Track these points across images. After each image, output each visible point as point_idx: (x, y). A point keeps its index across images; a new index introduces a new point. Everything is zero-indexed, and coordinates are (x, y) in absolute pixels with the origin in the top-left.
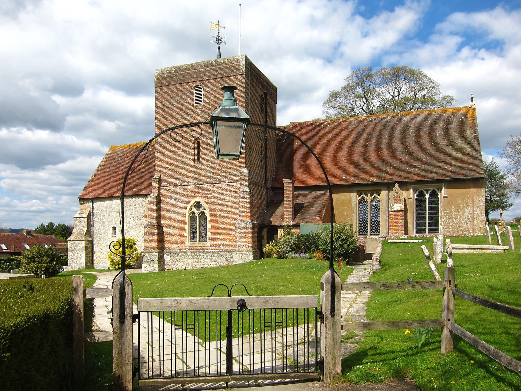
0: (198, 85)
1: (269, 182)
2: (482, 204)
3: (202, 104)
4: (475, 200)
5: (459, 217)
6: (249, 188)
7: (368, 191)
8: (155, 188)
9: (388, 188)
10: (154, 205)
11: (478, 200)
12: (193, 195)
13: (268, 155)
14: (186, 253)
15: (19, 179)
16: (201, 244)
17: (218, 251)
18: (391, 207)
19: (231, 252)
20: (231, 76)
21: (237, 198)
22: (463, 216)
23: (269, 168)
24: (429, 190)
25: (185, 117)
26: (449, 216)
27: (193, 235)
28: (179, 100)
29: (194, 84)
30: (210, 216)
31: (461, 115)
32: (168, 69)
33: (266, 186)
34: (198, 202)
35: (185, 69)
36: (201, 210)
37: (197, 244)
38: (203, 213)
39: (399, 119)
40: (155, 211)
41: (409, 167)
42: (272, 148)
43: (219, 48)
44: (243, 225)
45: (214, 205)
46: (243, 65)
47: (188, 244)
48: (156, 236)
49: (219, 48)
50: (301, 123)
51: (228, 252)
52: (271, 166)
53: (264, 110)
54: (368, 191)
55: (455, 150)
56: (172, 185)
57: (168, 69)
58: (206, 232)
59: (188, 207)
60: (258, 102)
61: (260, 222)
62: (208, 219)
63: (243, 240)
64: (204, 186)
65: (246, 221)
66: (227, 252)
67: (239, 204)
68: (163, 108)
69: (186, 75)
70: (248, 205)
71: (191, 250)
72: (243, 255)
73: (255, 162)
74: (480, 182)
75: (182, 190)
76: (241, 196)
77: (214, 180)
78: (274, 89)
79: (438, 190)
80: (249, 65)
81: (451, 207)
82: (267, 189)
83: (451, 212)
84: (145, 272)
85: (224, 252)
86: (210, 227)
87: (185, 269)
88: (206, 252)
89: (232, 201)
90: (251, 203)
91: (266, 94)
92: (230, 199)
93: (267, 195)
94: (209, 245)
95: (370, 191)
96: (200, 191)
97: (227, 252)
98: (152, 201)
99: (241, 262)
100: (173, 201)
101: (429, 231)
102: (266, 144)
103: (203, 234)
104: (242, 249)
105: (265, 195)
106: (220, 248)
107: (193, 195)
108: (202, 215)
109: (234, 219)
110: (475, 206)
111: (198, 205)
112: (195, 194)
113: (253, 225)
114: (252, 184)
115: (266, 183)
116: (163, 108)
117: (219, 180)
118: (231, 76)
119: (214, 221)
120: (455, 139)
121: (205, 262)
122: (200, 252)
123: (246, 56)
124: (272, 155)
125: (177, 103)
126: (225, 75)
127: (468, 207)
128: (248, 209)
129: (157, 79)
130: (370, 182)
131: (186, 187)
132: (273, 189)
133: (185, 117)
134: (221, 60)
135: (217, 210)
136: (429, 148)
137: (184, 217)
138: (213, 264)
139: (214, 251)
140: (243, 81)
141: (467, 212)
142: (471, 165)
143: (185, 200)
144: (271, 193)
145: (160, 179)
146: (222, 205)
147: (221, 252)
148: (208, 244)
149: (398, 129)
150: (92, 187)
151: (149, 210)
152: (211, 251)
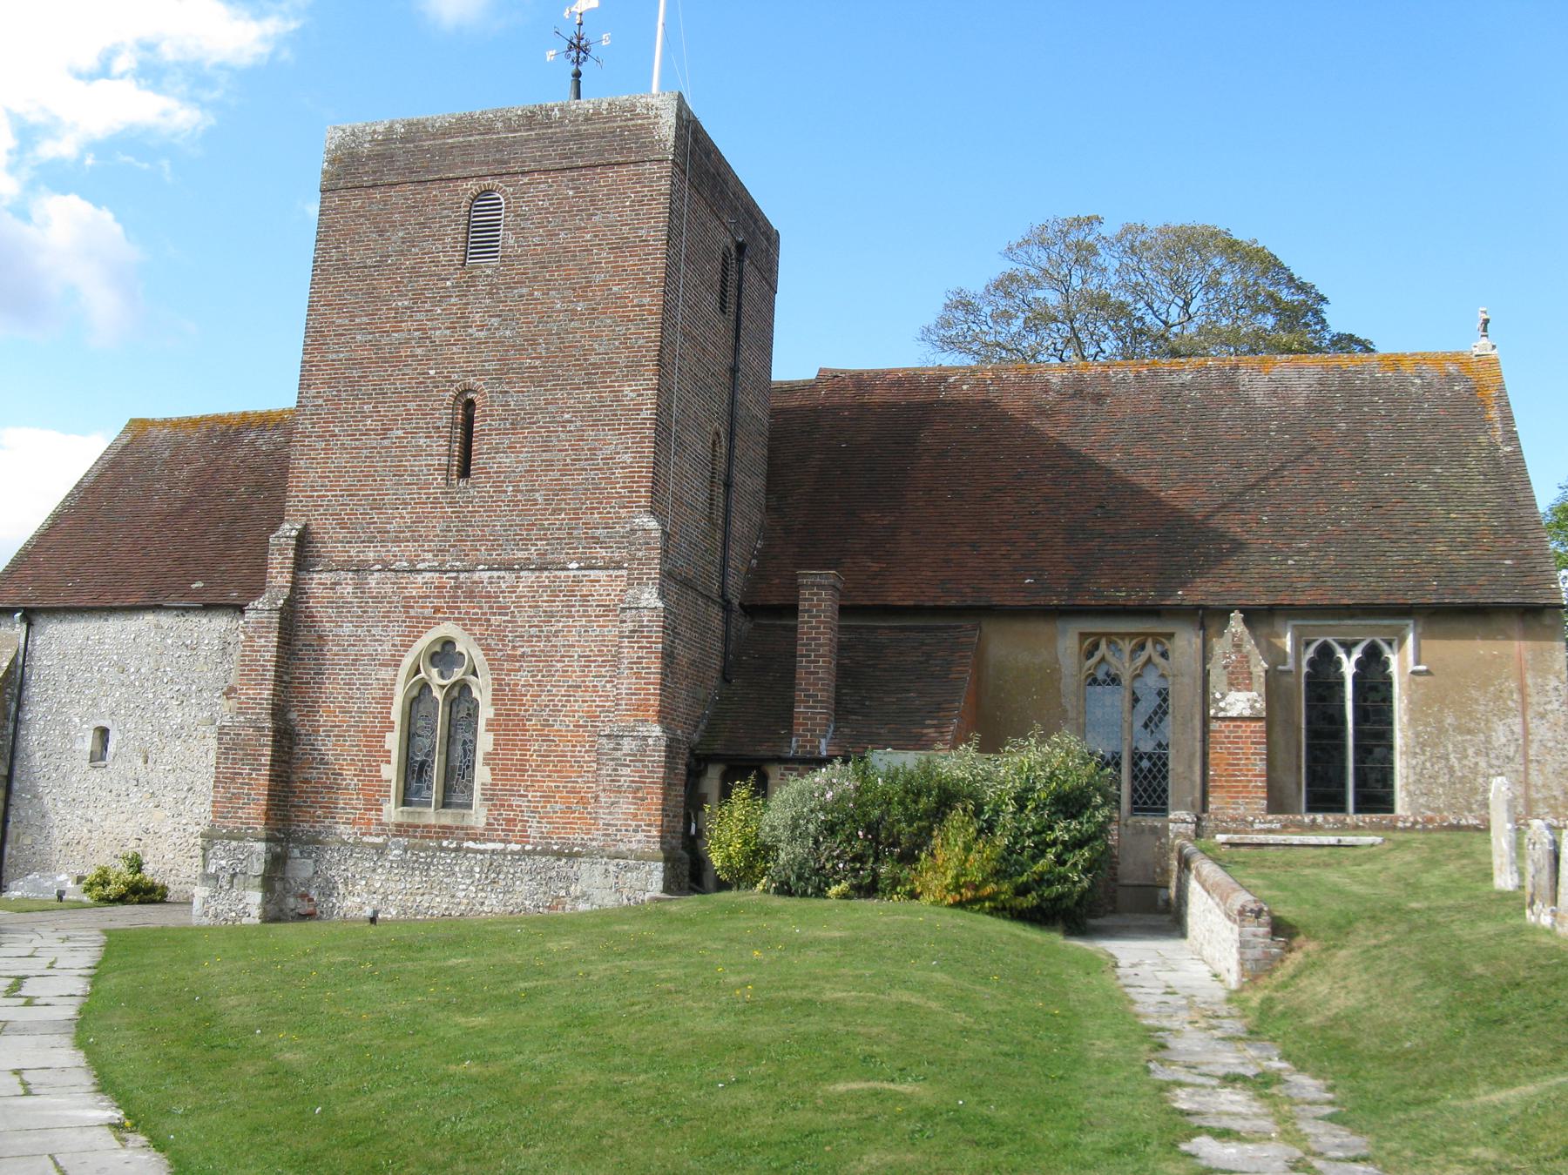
0: (488, 191)
1: (735, 583)
2: (1556, 705)
3: (495, 262)
4: (1531, 690)
5: (1471, 752)
6: (662, 595)
7: (1122, 636)
8: (279, 576)
9: (1203, 627)
10: (268, 645)
11: (1542, 691)
12: (428, 612)
13: (738, 477)
14: (381, 850)
15: (907, 912)
16: (447, 818)
17: (517, 847)
18: (1217, 701)
19: (572, 856)
20: (619, 164)
21: (612, 632)
22: (1486, 749)
23: (739, 526)
24: (1355, 644)
25: (427, 306)
26: (1435, 745)
27: (414, 771)
28: (410, 241)
29: (472, 186)
30: (495, 700)
31: (1451, 379)
32: (380, 129)
33: (723, 596)
34: (448, 643)
35: (446, 132)
36: (458, 673)
37: (431, 816)
38: (464, 687)
39: (1230, 383)
40: (270, 666)
41: (1278, 551)
42: (752, 453)
43: (577, 75)
44: (628, 745)
45: (512, 658)
46: (666, 128)
47: (392, 812)
48: (266, 771)
49: (577, 75)
50: (861, 373)
51: (559, 855)
52: (747, 520)
53: (733, 308)
54: (1122, 636)
55: (1445, 500)
56: (345, 566)
57: (380, 129)
58: (470, 766)
59: (407, 662)
60: (713, 270)
61: (696, 738)
62: (486, 712)
63: (626, 806)
64: (476, 576)
65: (642, 730)
66: (554, 853)
67: (617, 657)
68: (344, 266)
69: (446, 152)
70: (656, 667)
71: (404, 841)
72: (623, 875)
73: (687, 498)
74: (1547, 621)
75: (388, 588)
76: (629, 626)
77: (520, 554)
78: (771, 238)
79: (1390, 644)
80: (691, 133)
81: (1441, 710)
82: (726, 606)
83: (1441, 730)
84: (206, 921)
85: (544, 853)
86: (490, 748)
87: (373, 920)
88: (468, 850)
89: (588, 652)
90: (668, 657)
91: (741, 248)
92: (581, 635)
93: (727, 632)
94: (482, 822)
95: (1132, 635)
96: (458, 598)
97: (554, 853)
98: (260, 626)
99: (608, 900)
100: (347, 629)
101: (1356, 803)
102: (731, 435)
103: (454, 789)
104: (623, 847)
105: (719, 633)
106: (524, 838)
107: (428, 612)
108: (461, 694)
109: (593, 717)
110: (1530, 714)
111: (444, 654)
112: (437, 610)
113: (671, 749)
114: (674, 581)
115: (723, 585)
116: (344, 266)
117: (542, 555)
118: (619, 164)
119: (507, 725)
120: (1436, 460)
121: (462, 892)
122: (442, 849)
123: (680, 97)
124: (751, 482)
125: (402, 253)
126: (594, 160)
127: (1504, 713)
128: (655, 678)
129: (332, 162)
130: (1134, 600)
131: (405, 579)
132: (750, 610)
133: (427, 306)
134: (586, 104)
135: (523, 677)
136: (1346, 488)
137: (388, 699)
138: (492, 904)
139: (502, 846)
140: (665, 186)
141: (1500, 736)
142: (1505, 556)
143: (395, 630)
144: (743, 625)
145: (304, 540)
146: (546, 658)
147: (528, 853)
148: (478, 816)
149: (1224, 414)
150: (36, 565)
151: (249, 667)
152: (490, 846)
